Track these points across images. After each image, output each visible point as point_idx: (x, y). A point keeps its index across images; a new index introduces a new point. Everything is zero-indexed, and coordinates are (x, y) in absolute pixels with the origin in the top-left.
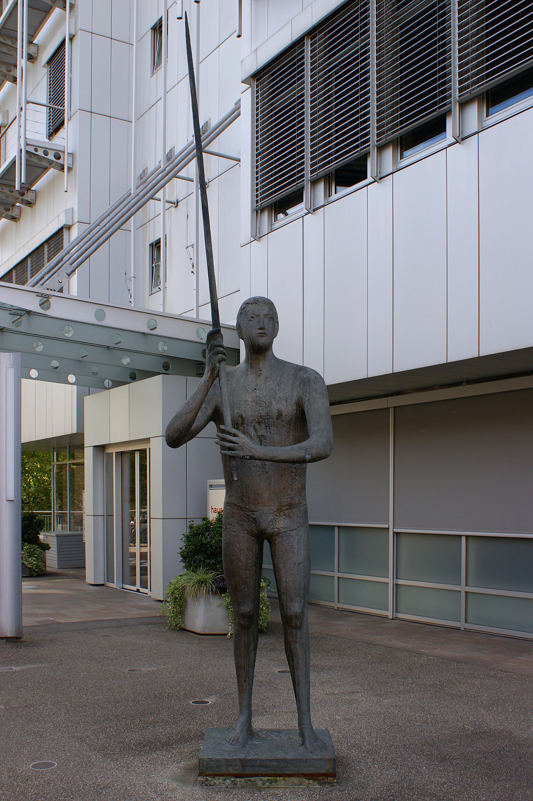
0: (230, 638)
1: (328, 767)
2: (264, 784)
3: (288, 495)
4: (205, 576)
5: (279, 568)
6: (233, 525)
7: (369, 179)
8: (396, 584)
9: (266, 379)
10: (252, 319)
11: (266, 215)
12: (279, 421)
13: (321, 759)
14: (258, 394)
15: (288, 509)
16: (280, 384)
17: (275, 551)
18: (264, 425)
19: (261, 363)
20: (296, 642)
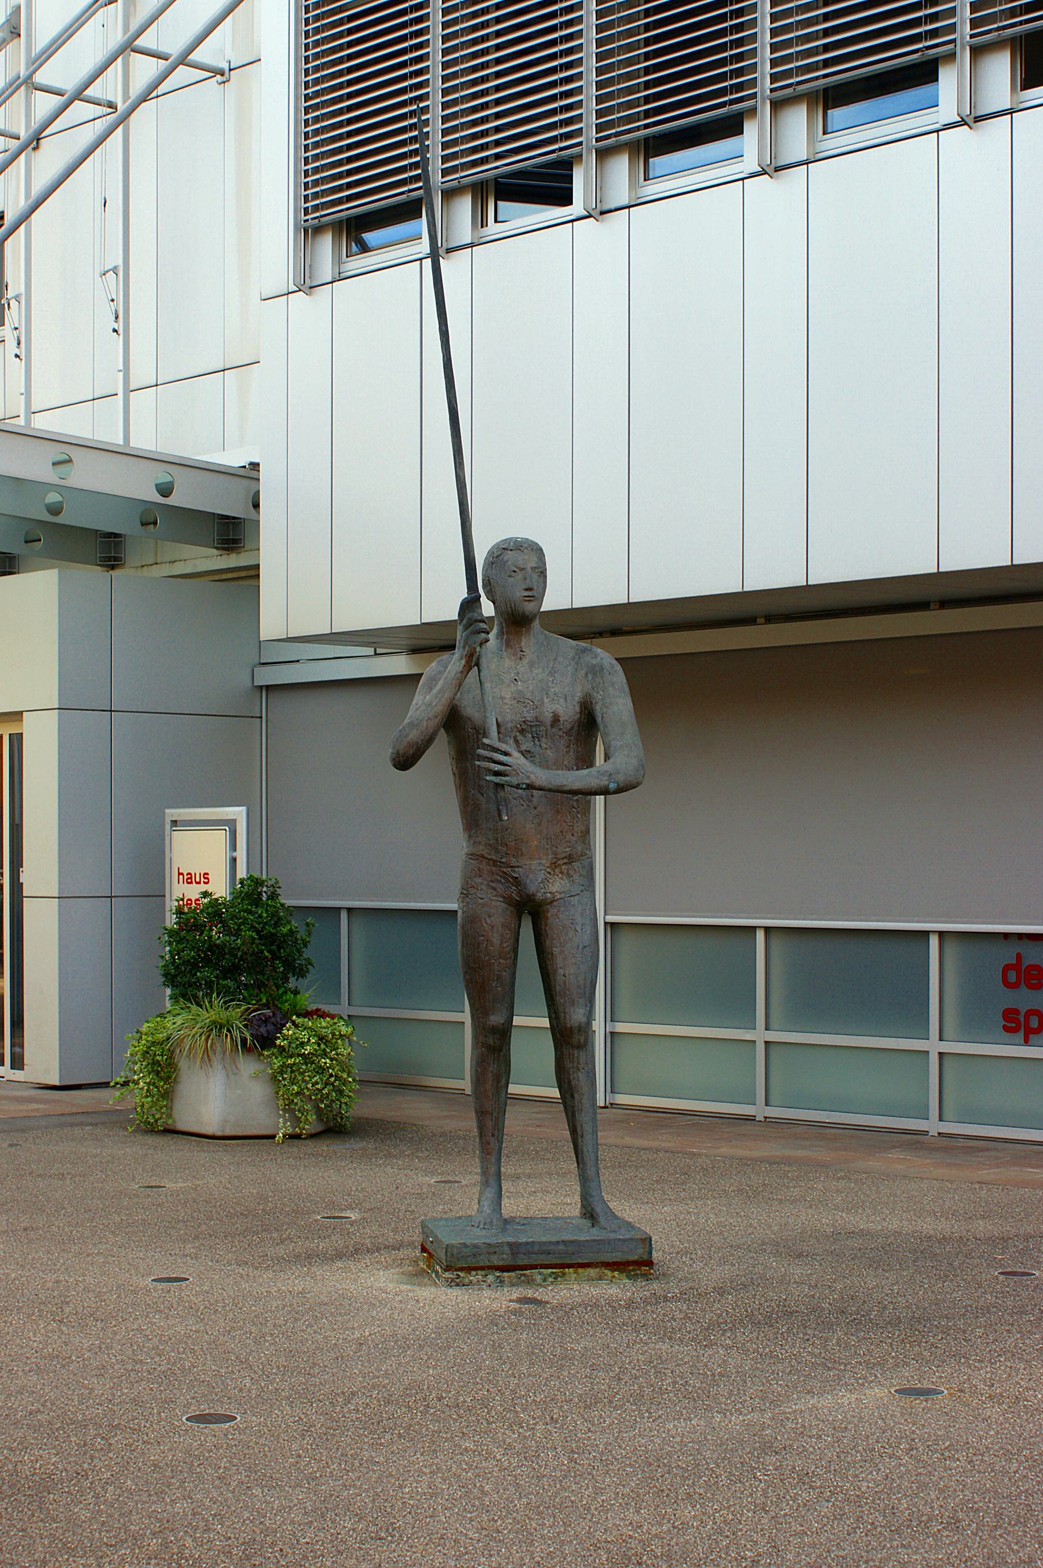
0: (283, 1142)
1: (641, 1251)
2: (545, 1280)
3: (566, 842)
4: (224, 1015)
5: (552, 954)
7: (577, 207)
8: (612, 1033)
9: (532, 665)
10: (513, 574)
11: (326, 242)
12: (553, 730)
13: (631, 1239)
14: (520, 688)
15: (566, 863)
16: (555, 672)
18: (530, 735)
19: (524, 640)
20: (579, 1069)
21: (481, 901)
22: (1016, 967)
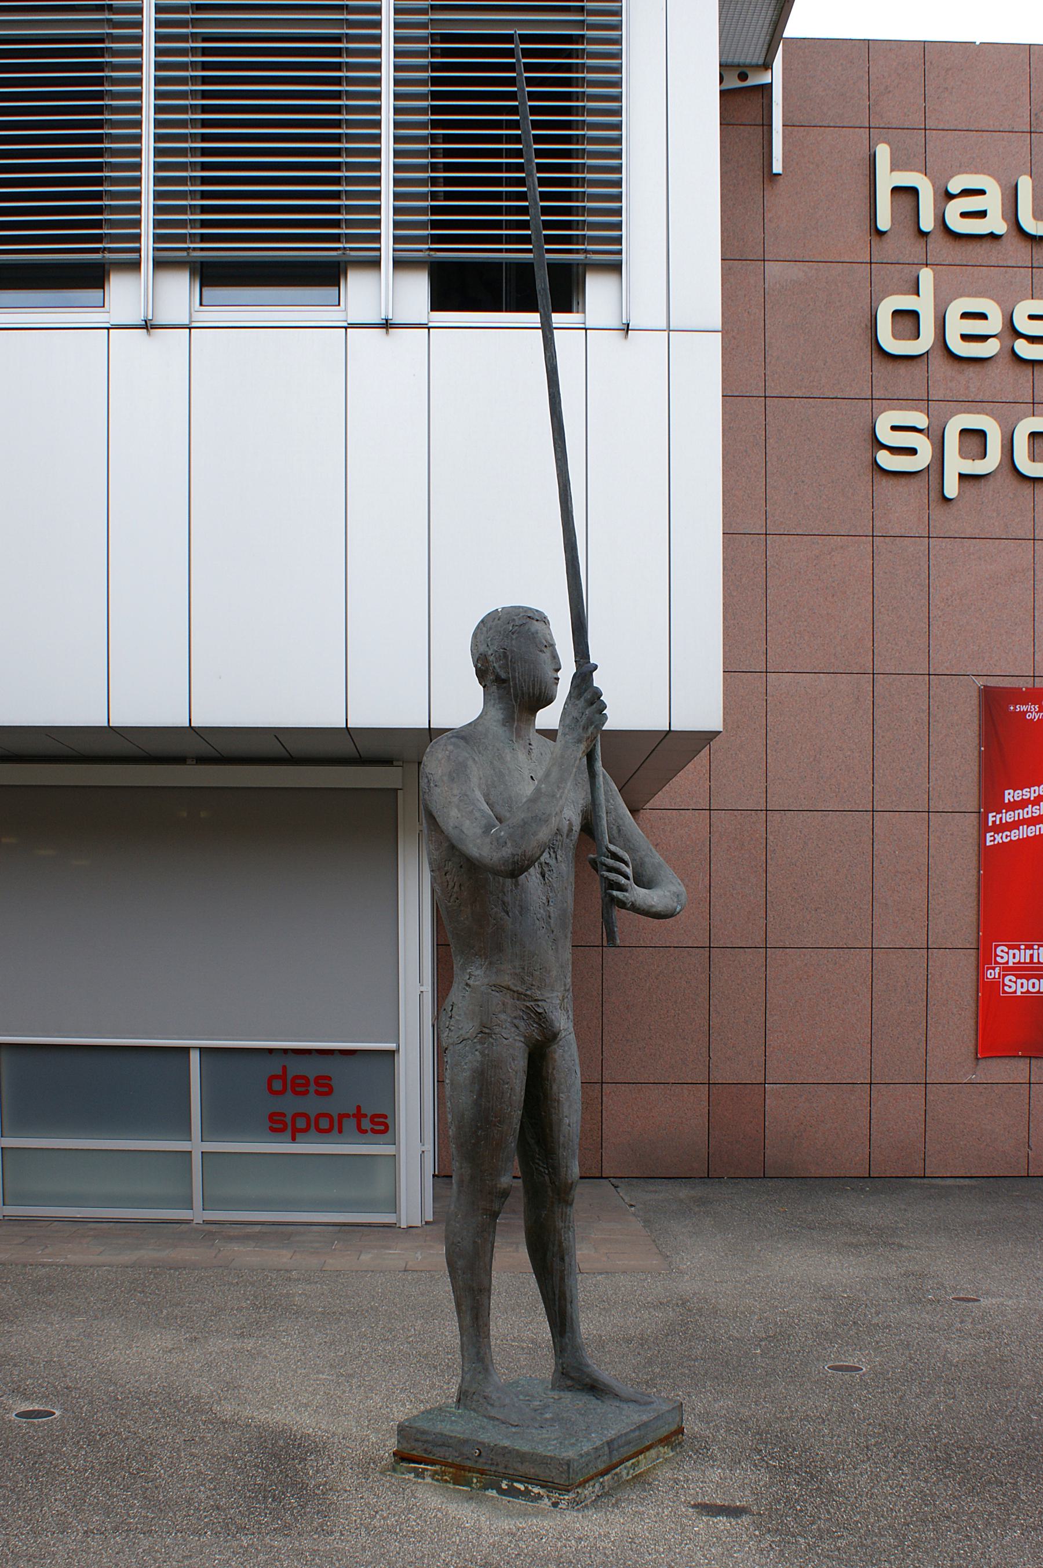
5: (558, 1101)
6: (504, 1026)
17: (555, 1072)
21: (506, 1042)
22: (283, 1077)
